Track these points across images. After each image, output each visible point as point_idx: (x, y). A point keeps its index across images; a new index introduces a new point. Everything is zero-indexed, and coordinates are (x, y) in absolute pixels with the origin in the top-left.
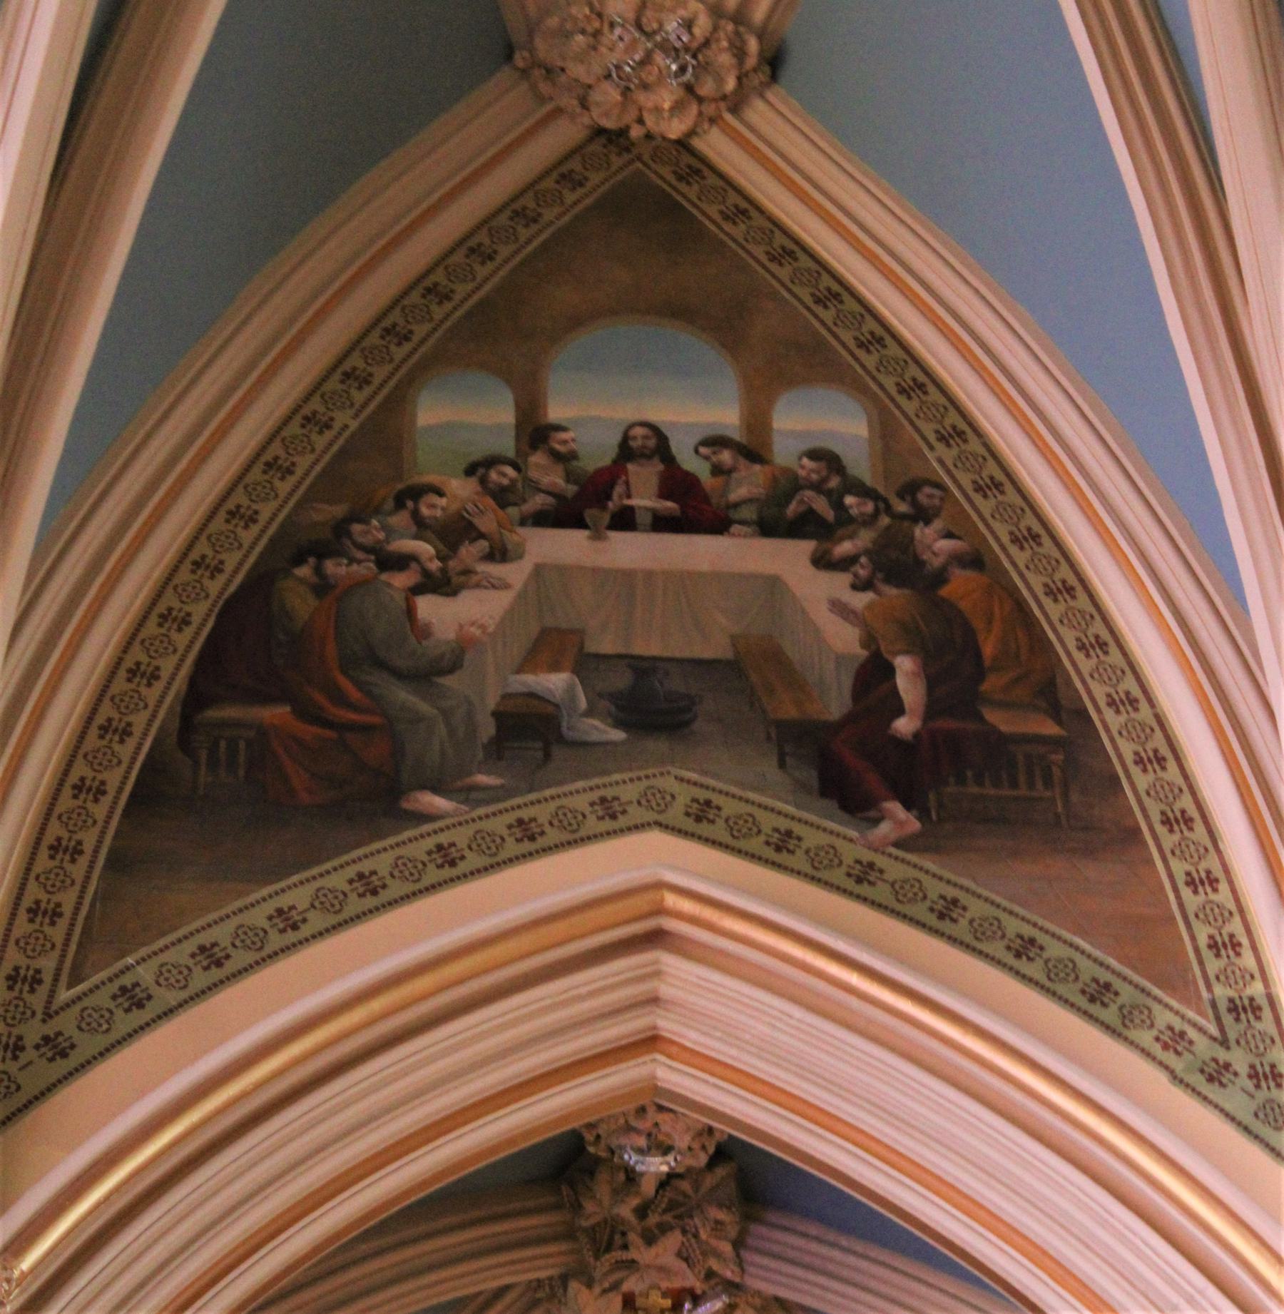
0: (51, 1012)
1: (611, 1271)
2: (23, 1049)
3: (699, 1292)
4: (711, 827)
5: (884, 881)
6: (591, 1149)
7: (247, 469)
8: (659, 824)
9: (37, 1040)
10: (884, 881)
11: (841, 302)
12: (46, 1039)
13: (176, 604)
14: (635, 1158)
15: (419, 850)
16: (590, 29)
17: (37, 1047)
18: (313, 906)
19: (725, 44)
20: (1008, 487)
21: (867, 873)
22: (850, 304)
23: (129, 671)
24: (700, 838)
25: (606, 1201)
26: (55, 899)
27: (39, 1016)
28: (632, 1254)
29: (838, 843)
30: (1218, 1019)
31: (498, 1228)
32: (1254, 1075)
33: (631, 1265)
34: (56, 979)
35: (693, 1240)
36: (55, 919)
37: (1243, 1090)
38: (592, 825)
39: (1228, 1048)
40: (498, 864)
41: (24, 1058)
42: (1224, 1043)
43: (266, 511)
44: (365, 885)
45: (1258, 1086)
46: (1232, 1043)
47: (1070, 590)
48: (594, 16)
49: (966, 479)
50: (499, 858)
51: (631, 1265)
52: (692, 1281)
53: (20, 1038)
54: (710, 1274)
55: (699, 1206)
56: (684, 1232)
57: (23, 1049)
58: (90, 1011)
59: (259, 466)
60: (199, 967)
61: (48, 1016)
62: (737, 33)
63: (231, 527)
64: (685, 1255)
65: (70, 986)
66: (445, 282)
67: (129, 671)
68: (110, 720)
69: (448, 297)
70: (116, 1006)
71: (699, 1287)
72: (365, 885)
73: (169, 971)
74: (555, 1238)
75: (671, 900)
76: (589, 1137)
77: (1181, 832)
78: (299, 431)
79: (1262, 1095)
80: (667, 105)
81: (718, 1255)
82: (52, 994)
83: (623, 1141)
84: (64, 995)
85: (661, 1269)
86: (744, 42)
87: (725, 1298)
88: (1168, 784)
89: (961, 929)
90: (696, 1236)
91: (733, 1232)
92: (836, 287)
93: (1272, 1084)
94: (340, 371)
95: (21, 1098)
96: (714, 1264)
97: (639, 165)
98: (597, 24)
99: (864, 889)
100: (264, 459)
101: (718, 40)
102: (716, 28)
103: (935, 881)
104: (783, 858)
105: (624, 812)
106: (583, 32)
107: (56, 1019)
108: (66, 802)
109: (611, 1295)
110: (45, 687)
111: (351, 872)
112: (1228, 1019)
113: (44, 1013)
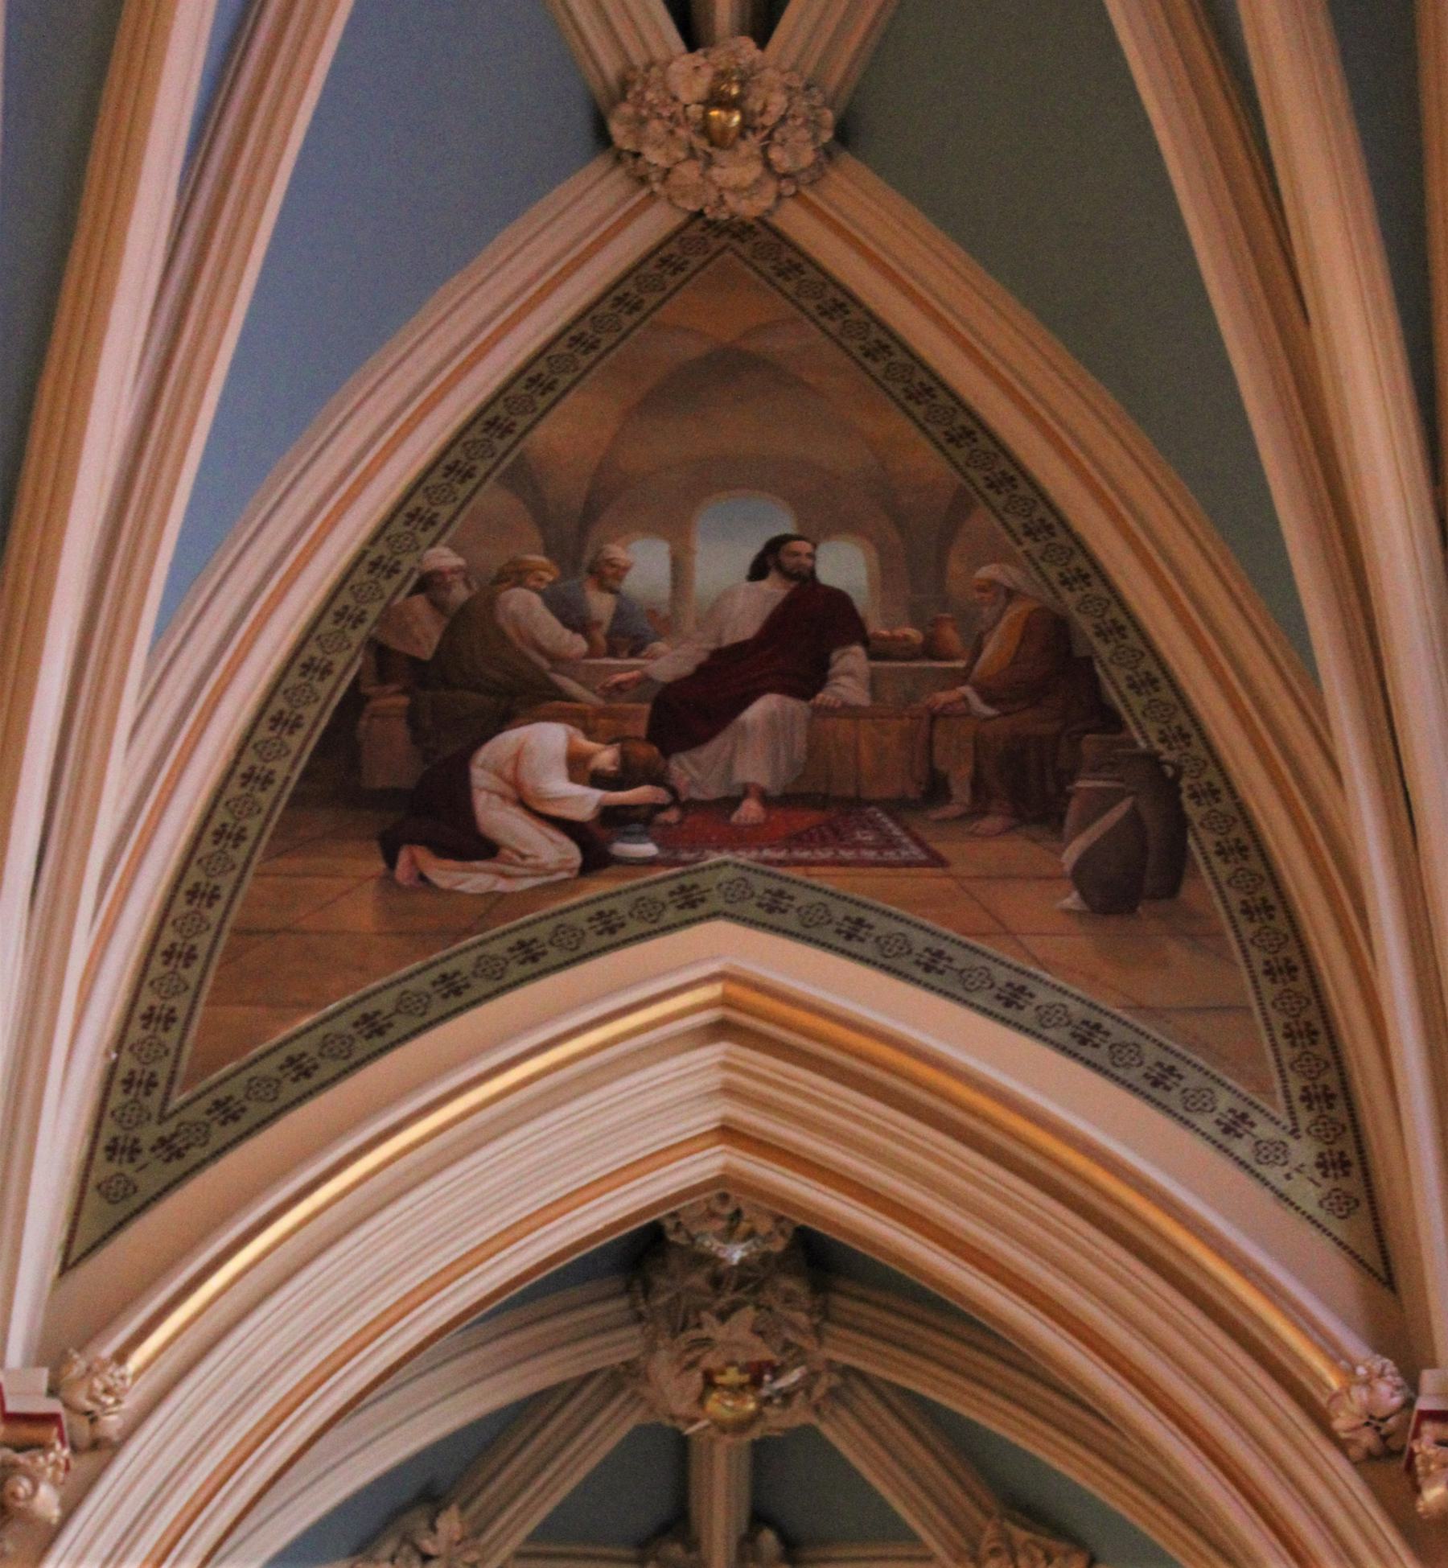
1: (689, 1350)
2: (139, 1151)
5: (952, 968)
6: (672, 1238)
10: (952, 968)
14: (717, 1244)
17: (153, 1149)
27: (155, 1118)
33: (706, 1342)
34: (171, 1081)
41: (141, 1160)
44: (224, 1113)
51: (706, 1342)
52: (764, 1352)
53: (136, 1141)
54: (788, 1345)
56: (758, 1307)
57: (139, 1151)
61: (163, 1119)
65: (183, 1090)
66: (590, 332)
71: (777, 1360)
72: (224, 1113)
76: (669, 1225)
81: (793, 1326)
83: (705, 1228)
84: (178, 1099)
89: (1027, 1016)
90: (770, 1309)
94: (526, 376)
95: (136, 1201)
96: (790, 1335)
106: (660, 117)
108: (181, 907)
110: (162, 791)
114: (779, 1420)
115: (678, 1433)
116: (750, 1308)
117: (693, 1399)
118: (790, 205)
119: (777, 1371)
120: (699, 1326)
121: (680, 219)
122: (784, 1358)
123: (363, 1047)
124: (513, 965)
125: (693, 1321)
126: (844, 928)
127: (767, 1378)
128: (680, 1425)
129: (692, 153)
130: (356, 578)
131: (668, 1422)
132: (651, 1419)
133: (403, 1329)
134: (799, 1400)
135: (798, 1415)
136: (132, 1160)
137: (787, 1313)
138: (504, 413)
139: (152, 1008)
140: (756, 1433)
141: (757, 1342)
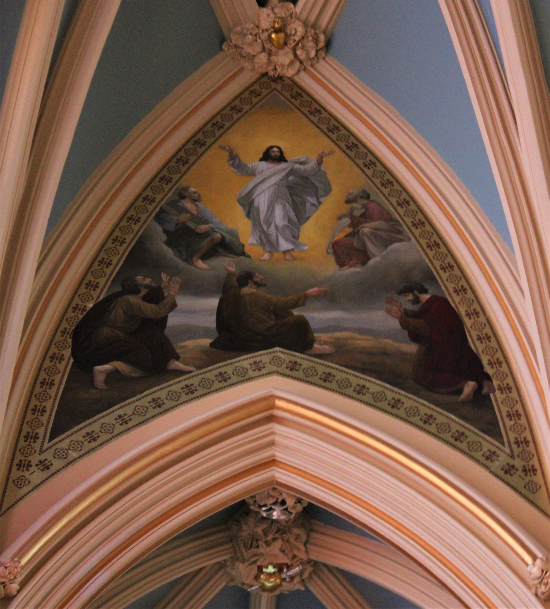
0: (43, 450)
2: (31, 466)
3: (289, 564)
4: (297, 373)
6: (252, 508)
7: (120, 220)
8: (278, 373)
9: (37, 462)
11: (358, 148)
12: (41, 462)
13: (93, 279)
15: (177, 388)
16: (254, 33)
17: (37, 465)
18: (134, 413)
19: (311, 38)
20: (427, 224)
21: (361, 390)
22: (362, 149)
23: (74, 308)
24: (292, 377)
25: (252, 526)
26: (43, 404)
27: (38, 452)
28: (261, 550)
29: (350, 378)
30: (510, 447)
31: (210, 538)
32: (525, 470)
35: (287, 544)
36: (43, 413)
37: (519, 476)
38: (251, 373)
39: (514, 459)
40: (211, 392)
41: (31, 470)
42: (512, 457)
43: (129, 238)
45: (526, 475)
46: (516, 456)
47: (451, 267)
48: (255, 28)
49: (409, 221)
50: (114, 434)
52: (285, 560)
53: (30, 462)
54: (294, 557)
55: (289, 529)
58: (106, 425)
59: (158, 179)
60: (151, 407)
61: (41, 452)
62: (316, 33)
63: (194, 147)
64: (283, 550)
67: (74, 308)
68: (65, 329)
69: (153, 201)
70: (150, 406)
71: (289, 563)
72: (122, 420)
73: (139, 409)
74: (223, 544)
75: (279, 403)
77: (497, 368)
78: (158, 184)
79: (528, 479)
80: (287, 63)
81: (299, 549)
82: (42, 444)
84: (46, 446)
85: (274, 555)
86: (318, 37)
87: (301, 567)
88: (491, 348)
91: (304, 538)
92: (356, 142)
93: (532, 474)
96: (296, 552)
97: (275, 91)
98: (257, 31)
99: (361, 397)
100: (159, 176)
101: (308, 37)
102: (306, 32)
103: (390, 392)
104: (327, 384)
105: (264, 367)
106: (251, 34)
107: (45, 453)
109: (253, 566)
111: (149, 398)
112: (514, 447)
113: (40, 451)
114: (287, 587)
115: (246, 591)
116: (280, 541)
117: (253, 577)
118: (303, 74)
119: (289, 567)
120: (258, 547)
121: (258, 75)
122: (293, 562)
123: (184, 398)
124: (183, 395)
125: (255, 544)
126: (332, 377)
127: (285, 570)
128: (245, 587)
129: (264, 49)
130: (170, 165)
131: (240, 585)
132: (232, 584)
133: (423, 553)
134: (297, 580)
135: (297, 586)
136: (28, 470)
137: (295, 543)
138: (120, 235)
139: (36, 406)
140: (277, 592)
141: (282, 555)
